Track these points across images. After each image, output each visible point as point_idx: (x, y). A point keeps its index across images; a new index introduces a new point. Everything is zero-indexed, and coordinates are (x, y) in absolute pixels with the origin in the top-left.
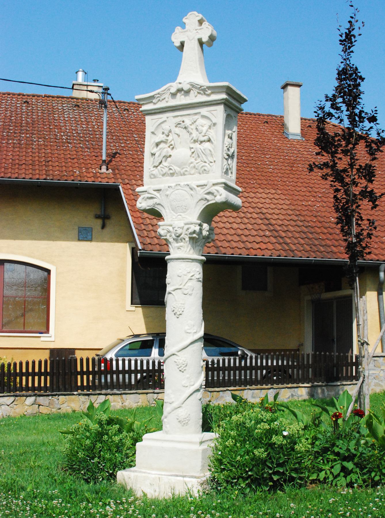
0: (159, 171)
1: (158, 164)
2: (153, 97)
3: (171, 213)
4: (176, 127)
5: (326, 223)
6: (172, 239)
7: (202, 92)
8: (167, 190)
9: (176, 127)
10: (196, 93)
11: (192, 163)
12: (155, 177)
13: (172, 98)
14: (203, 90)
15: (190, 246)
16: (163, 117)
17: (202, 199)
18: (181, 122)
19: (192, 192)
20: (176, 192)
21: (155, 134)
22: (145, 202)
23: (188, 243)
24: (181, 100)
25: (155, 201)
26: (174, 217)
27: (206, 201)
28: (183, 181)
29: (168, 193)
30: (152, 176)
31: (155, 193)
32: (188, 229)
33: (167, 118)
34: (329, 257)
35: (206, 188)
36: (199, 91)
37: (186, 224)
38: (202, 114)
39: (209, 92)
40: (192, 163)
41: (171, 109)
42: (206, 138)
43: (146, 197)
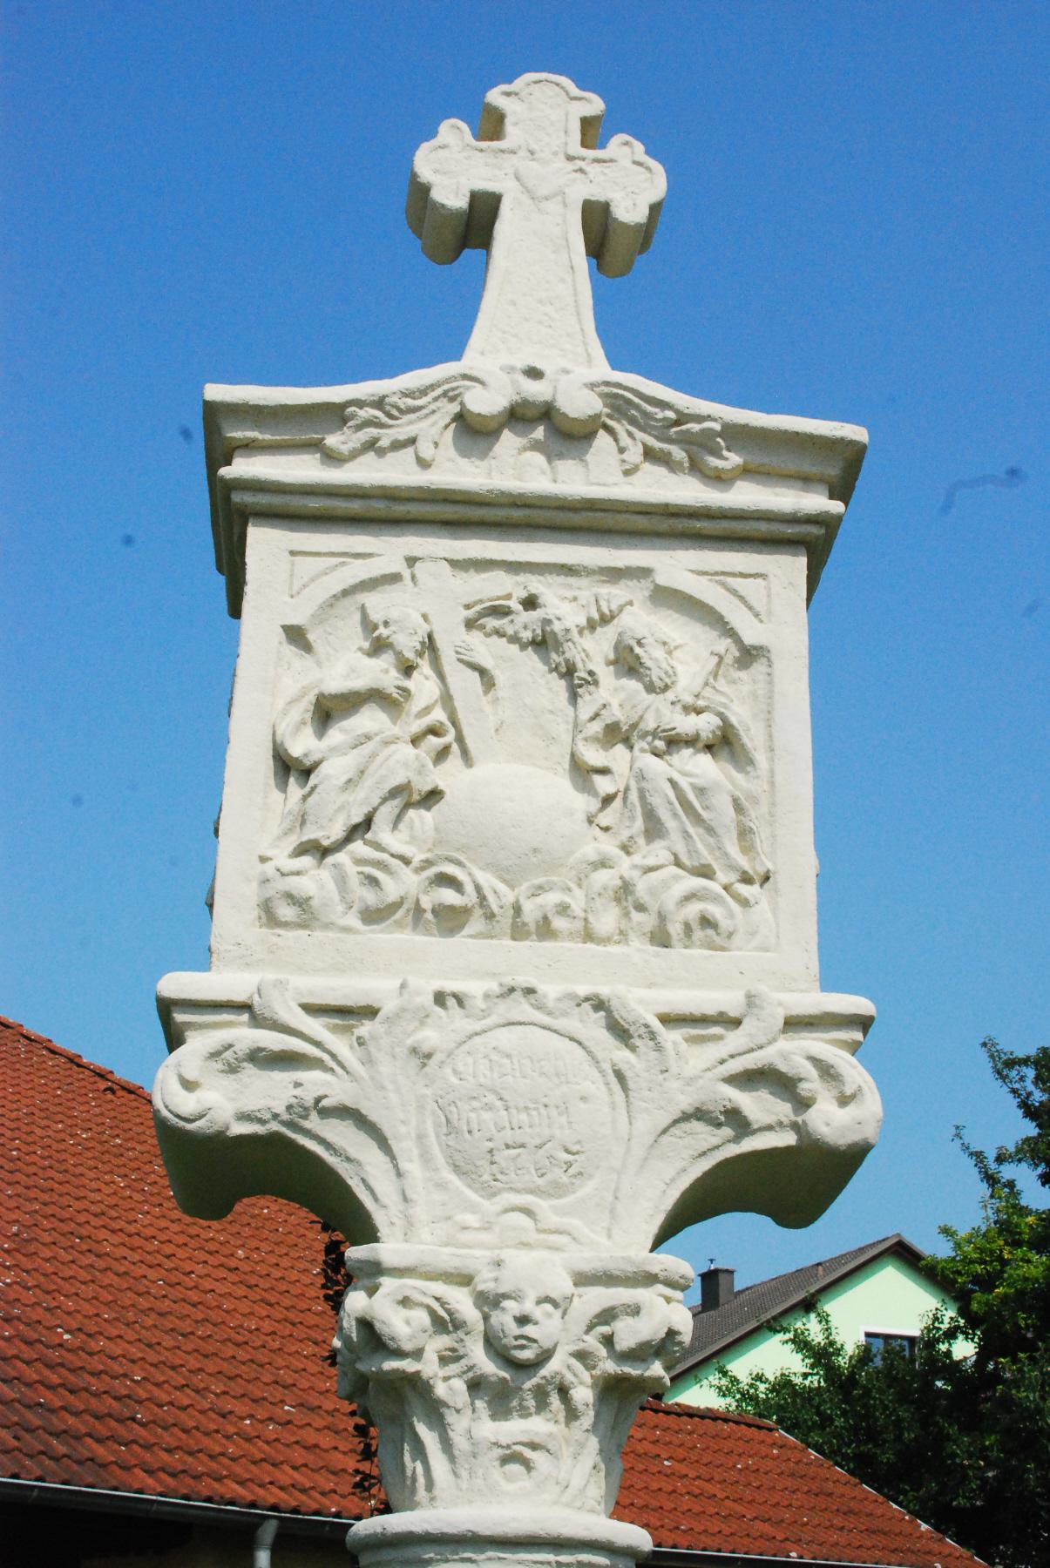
0: (341, 880)
1: (337, 831)
2: (337, 415)
3: (441, 1186)
4: (470, 624)
5: (48, 1347)
6: (460, 1385)
7: (678, 453)
8: (424, 1019)
9: (470, 624)
10: (635, 454)
11: (603, 863)
12: (306, 913)
13: (464, 452)
14: (686, 441)
15: (593, 1443)
16: (388, 550)
17: (700, 1114)
18: (514, 604)
19: (622, 1055)
20: (505, 1037)
21: (307, 647)
22: (228, 1081)
23: (587, 1420)
24: (516, 468)
25: (314, 1082)
26: (472, 1220)
27: (727, 1132)
28: (564, 971)
29: (429, 1037)
30: (286, 912)
31: (315, 1026)
32: (608, 1316)
33: (411, 561)
34: (90, 1480)
35: (734, 1040)
36: (657, 445)
37: (584, 1279)
38: (661, 580)
39: (734, 459)
40: (603, 863)
41: (449, 512)
42: (705, 725)
43: (242, 1047)
